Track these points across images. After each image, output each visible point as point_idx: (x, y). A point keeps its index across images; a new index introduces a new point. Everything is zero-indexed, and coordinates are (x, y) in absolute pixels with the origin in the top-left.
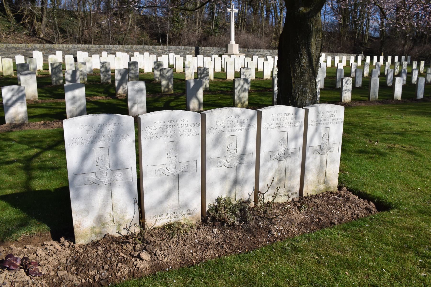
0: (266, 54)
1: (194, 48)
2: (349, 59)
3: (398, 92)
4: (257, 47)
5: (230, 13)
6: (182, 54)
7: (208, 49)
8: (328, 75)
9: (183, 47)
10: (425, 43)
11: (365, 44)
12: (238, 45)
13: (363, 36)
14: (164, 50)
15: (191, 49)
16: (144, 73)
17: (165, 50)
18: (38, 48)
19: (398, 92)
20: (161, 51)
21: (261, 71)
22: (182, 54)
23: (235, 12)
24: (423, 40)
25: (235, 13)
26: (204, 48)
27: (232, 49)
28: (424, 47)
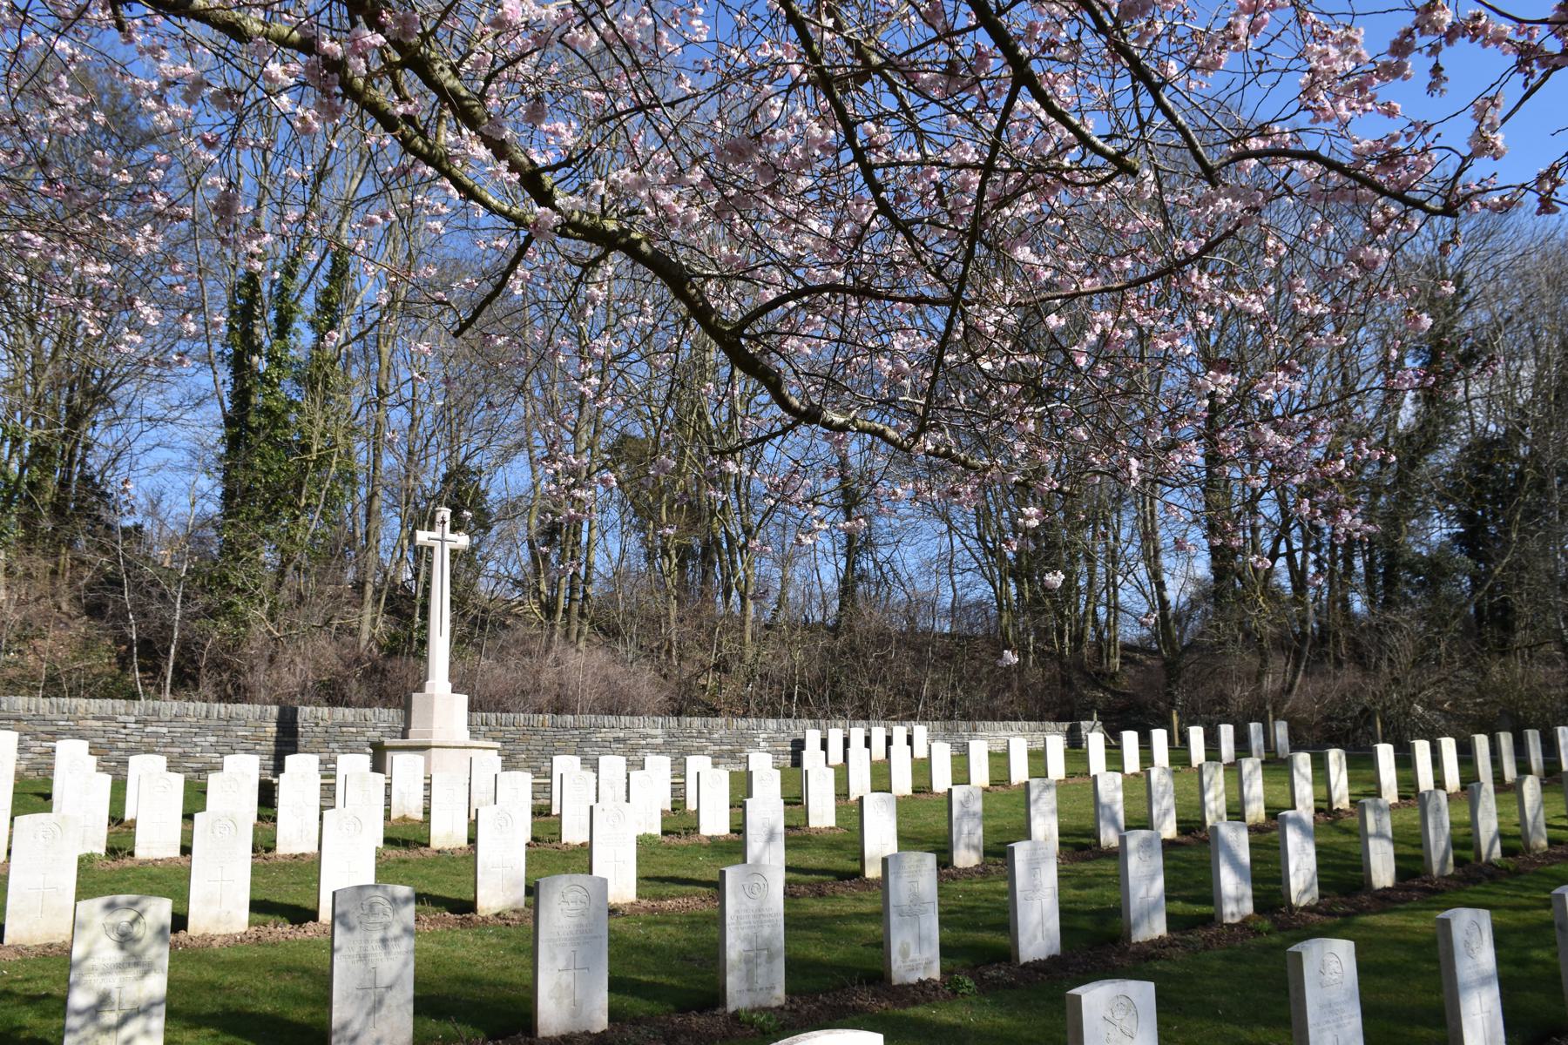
0: (645, 737)
1: (274, 710)
2: (796, 793)
3: (1383, 870)
4: (615, 705)
5: (431, 549)
6: (213, 739)
7: (351, 719)
8: (188, 973)
9: (220, 708)
10: (1339, 663)
11: (1113, 676)
12: (463, 699)
13: (1101, 647)
14: (113, 719)
15: (262, 718)
16: (127, 862)
17: (121, 719)
18: (853, 569)
19: (1383, 870)
20: (100, 723)
21: (578, 841)
22: (213, 739)
23: (455, 546)
24: (1328, 654)
25: (453, 552)
26: (331, 714)
27: (429, 720)
28: (1335, 677)
